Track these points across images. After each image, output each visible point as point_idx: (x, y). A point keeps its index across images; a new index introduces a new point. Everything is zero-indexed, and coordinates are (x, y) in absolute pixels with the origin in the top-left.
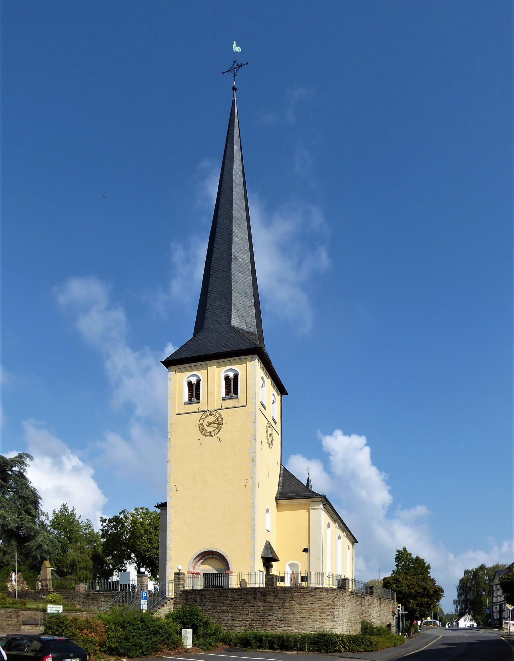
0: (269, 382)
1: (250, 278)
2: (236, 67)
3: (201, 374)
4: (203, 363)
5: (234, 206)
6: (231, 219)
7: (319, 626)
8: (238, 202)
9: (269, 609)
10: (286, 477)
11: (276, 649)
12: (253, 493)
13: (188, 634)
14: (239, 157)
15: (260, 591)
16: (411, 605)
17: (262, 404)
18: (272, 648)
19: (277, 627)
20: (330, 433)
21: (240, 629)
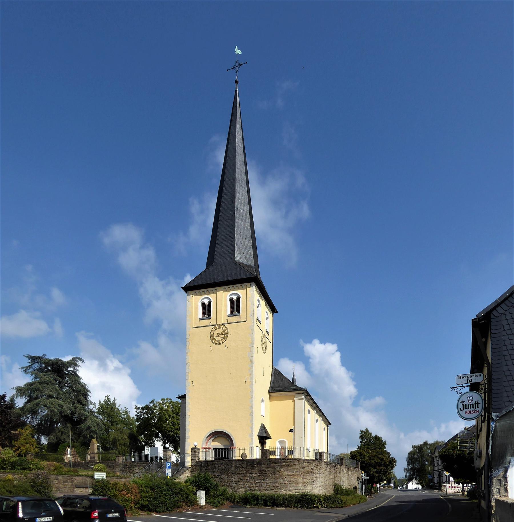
0: (263, 303)
1: (249, 224)
2: (238, 66)
3: (212, 297)
4: (213, 289)
5: (237, 170)
6: (234, 180)
7: (302, 488)
8: (240, 167)
9: (263, 475)
10: (277, 375)
11: (269, 506)
12: (252, 388)
13: (202, 495)
14: (240, 133)
15: (257, 462)
16: (372, 472)
17: (258, 320)
18: (266, 505)
19: (269, 489)
20: (309, 341)
21: (241, 491)
